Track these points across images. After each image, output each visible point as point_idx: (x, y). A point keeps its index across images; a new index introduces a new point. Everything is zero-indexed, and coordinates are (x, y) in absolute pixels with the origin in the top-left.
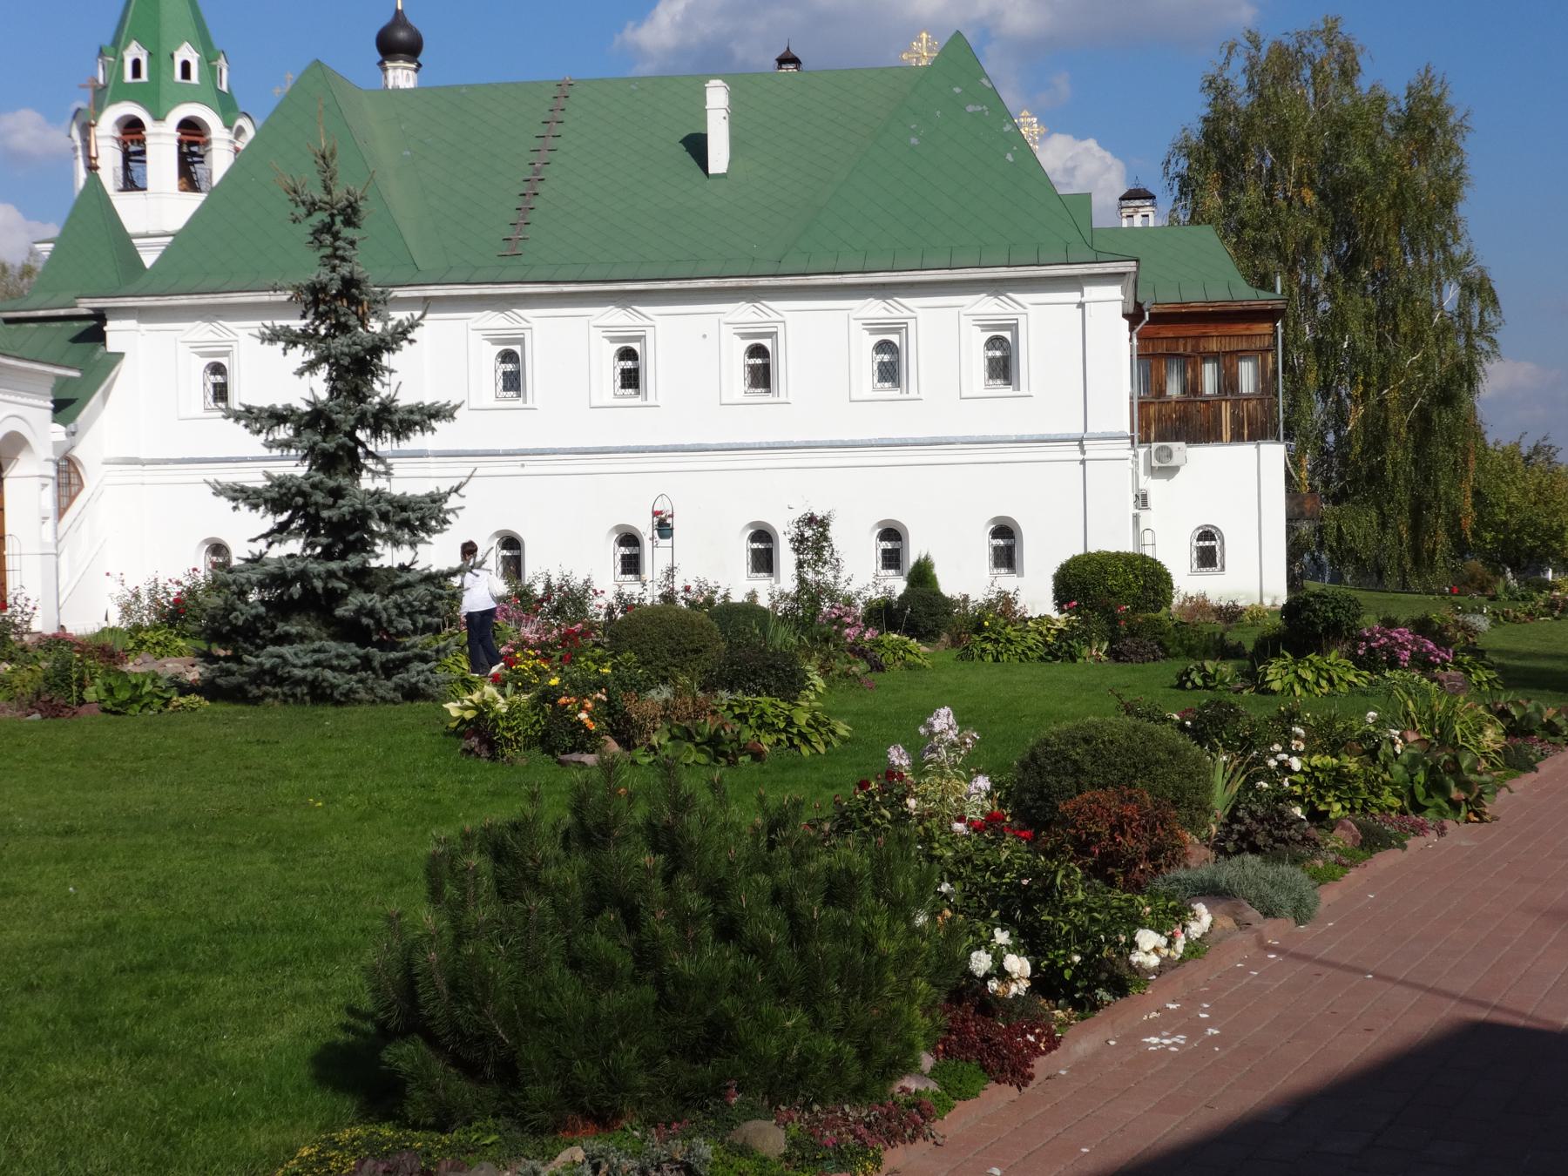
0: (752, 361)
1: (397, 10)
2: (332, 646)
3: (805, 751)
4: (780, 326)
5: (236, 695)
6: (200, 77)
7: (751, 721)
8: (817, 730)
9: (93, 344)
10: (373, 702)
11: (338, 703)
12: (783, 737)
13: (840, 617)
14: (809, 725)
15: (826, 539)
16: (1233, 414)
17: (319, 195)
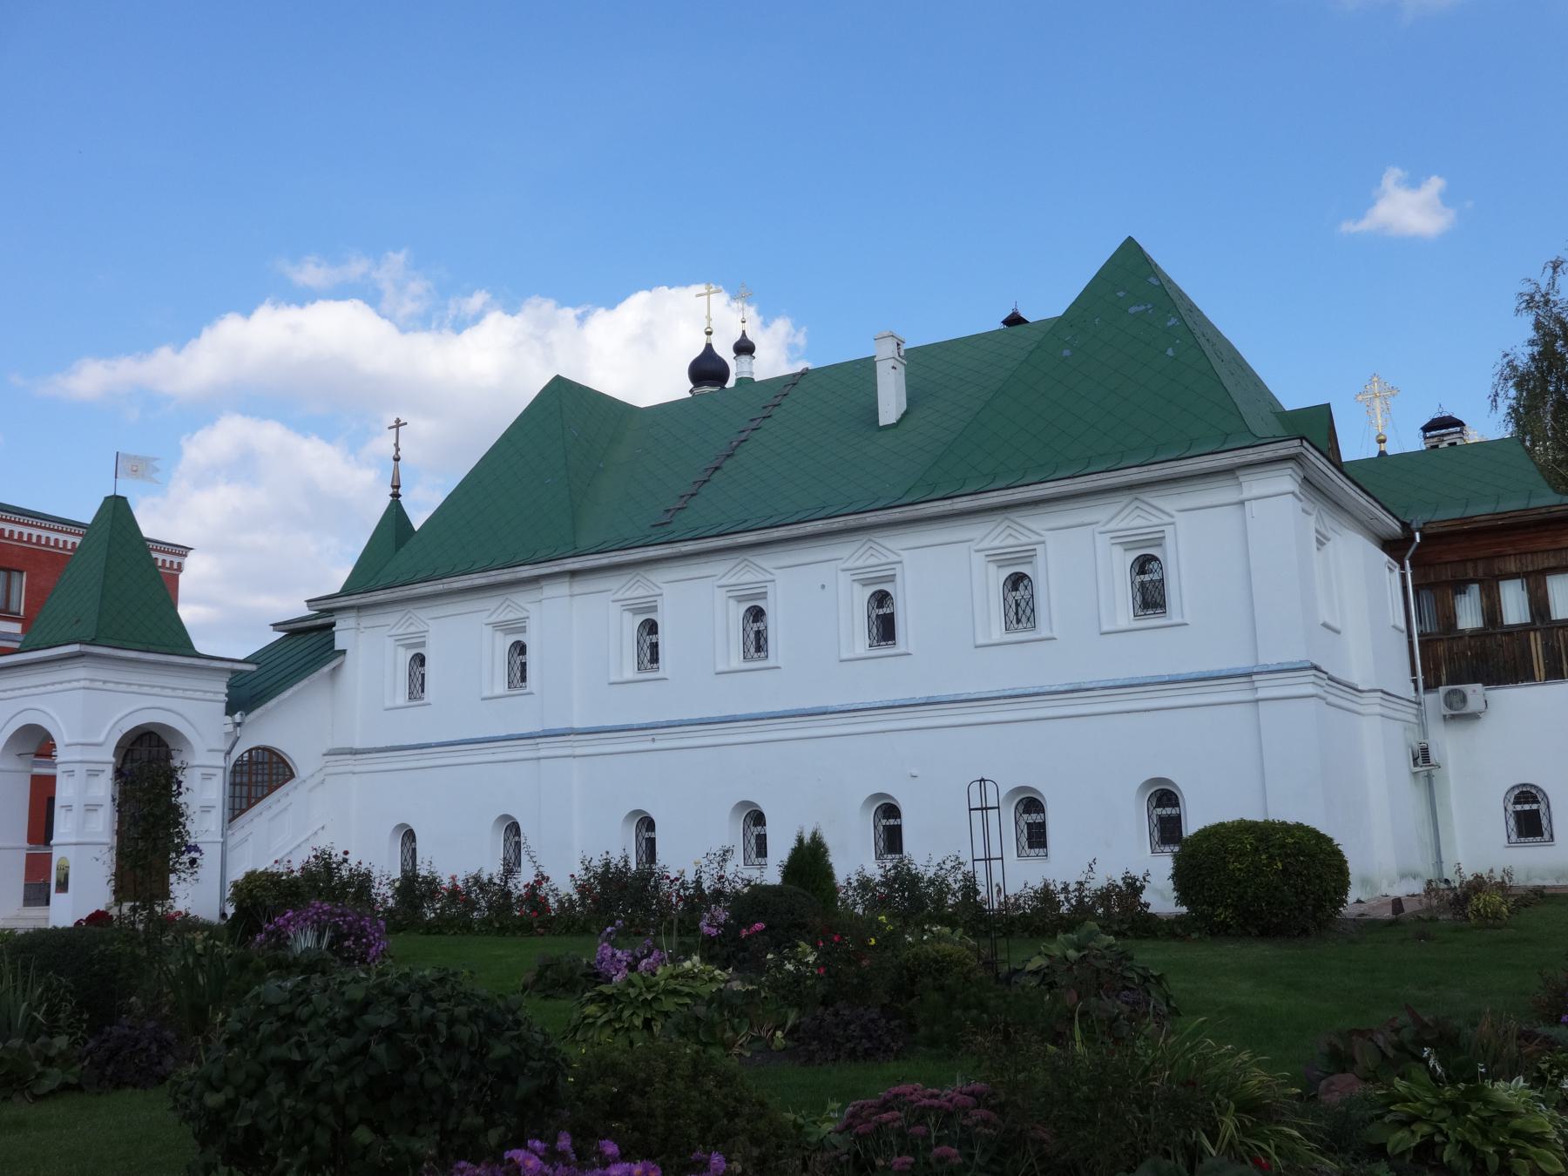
16: (1545, 646)
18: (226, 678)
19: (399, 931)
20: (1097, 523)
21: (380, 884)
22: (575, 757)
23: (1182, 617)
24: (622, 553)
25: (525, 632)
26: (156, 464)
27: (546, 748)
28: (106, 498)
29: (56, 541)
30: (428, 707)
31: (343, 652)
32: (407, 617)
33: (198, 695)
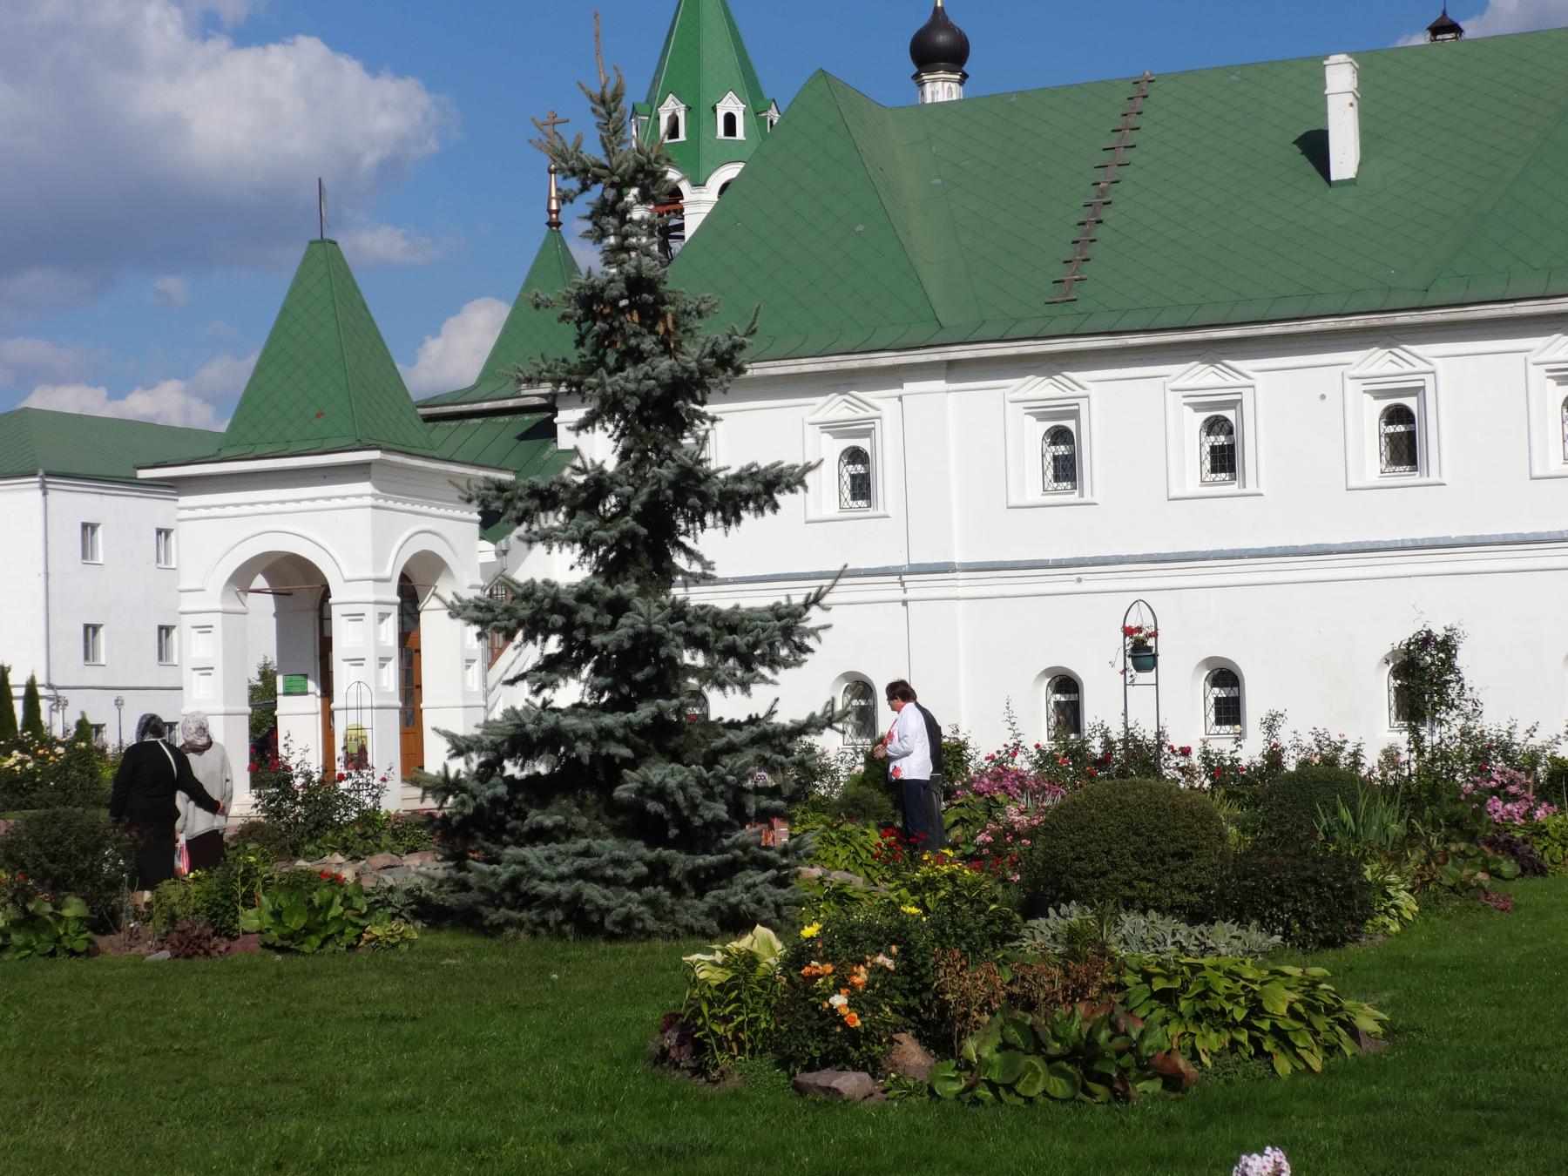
0: (1391, 429)
1: (936, 8)
2: (610, 846)
3: (1283, 1065)
4: (1429, 378)
5: (467, 920)
6: (746, 133)
7: (1183, 1005)
8: (1309, 1024)
9: (543, 441)
10: (676, 936)
11: (612, 937)
12: (1243, 1037)
13: (1503, 786)
14: (1292, 1011)
15: (1452, 669)
17: (593, 151)
20: (1350, 364)
23: (1440, 476)
27: (918, 587)
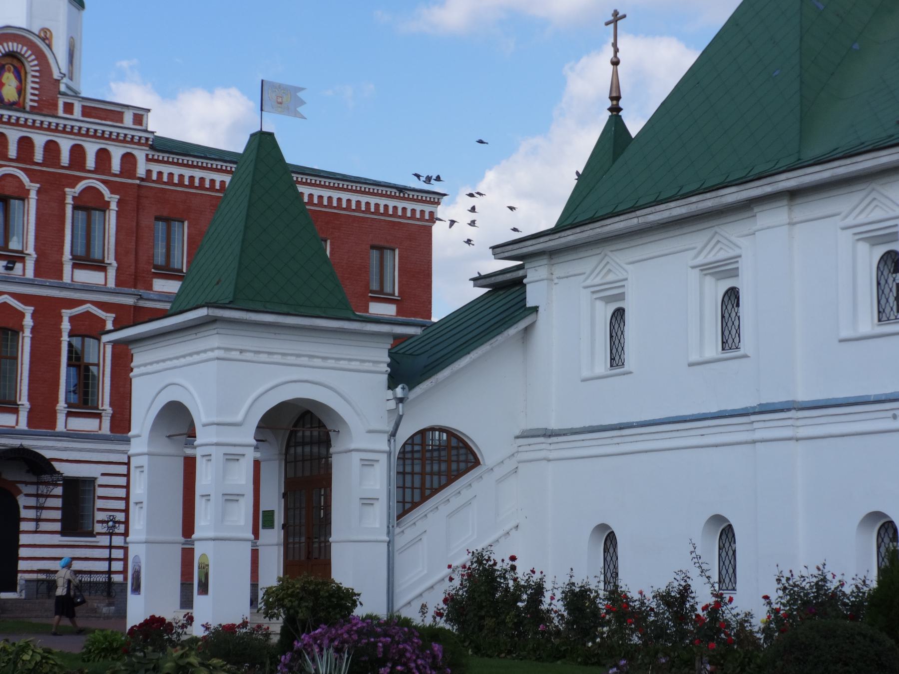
18: (388, 344)
19: (559, 659)
21: (552, 598)
22: (797, 440)
24: (848, 161)
25: (737, 276)
26: (300, 94)
28: (252, 136)
29: (358, 203)
30: (629, 375)
31: (535, 309)
32: (604, 262)
33: (355, 365)
